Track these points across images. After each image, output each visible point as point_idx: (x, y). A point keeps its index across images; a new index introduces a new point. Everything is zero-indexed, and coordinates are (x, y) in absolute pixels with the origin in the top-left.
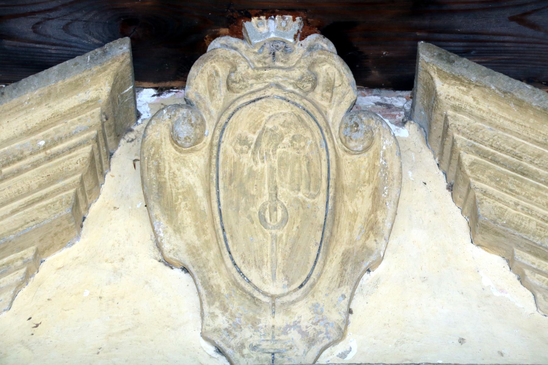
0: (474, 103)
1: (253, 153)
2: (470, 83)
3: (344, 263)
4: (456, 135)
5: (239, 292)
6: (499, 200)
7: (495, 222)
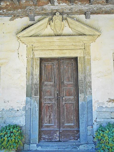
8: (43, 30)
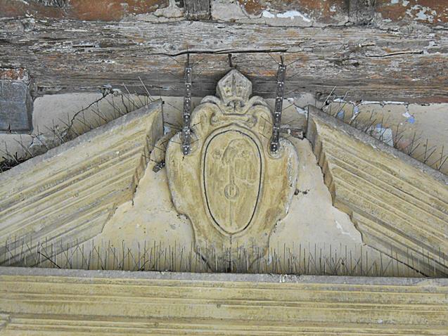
0: (335, 138)
1: (222, 159)
2: (334, 128)
3: (267, 216)
4: (326, 154)
5: (213, 230)
6: (346, 188)
7: (343, 199)
8: (99, 213)
